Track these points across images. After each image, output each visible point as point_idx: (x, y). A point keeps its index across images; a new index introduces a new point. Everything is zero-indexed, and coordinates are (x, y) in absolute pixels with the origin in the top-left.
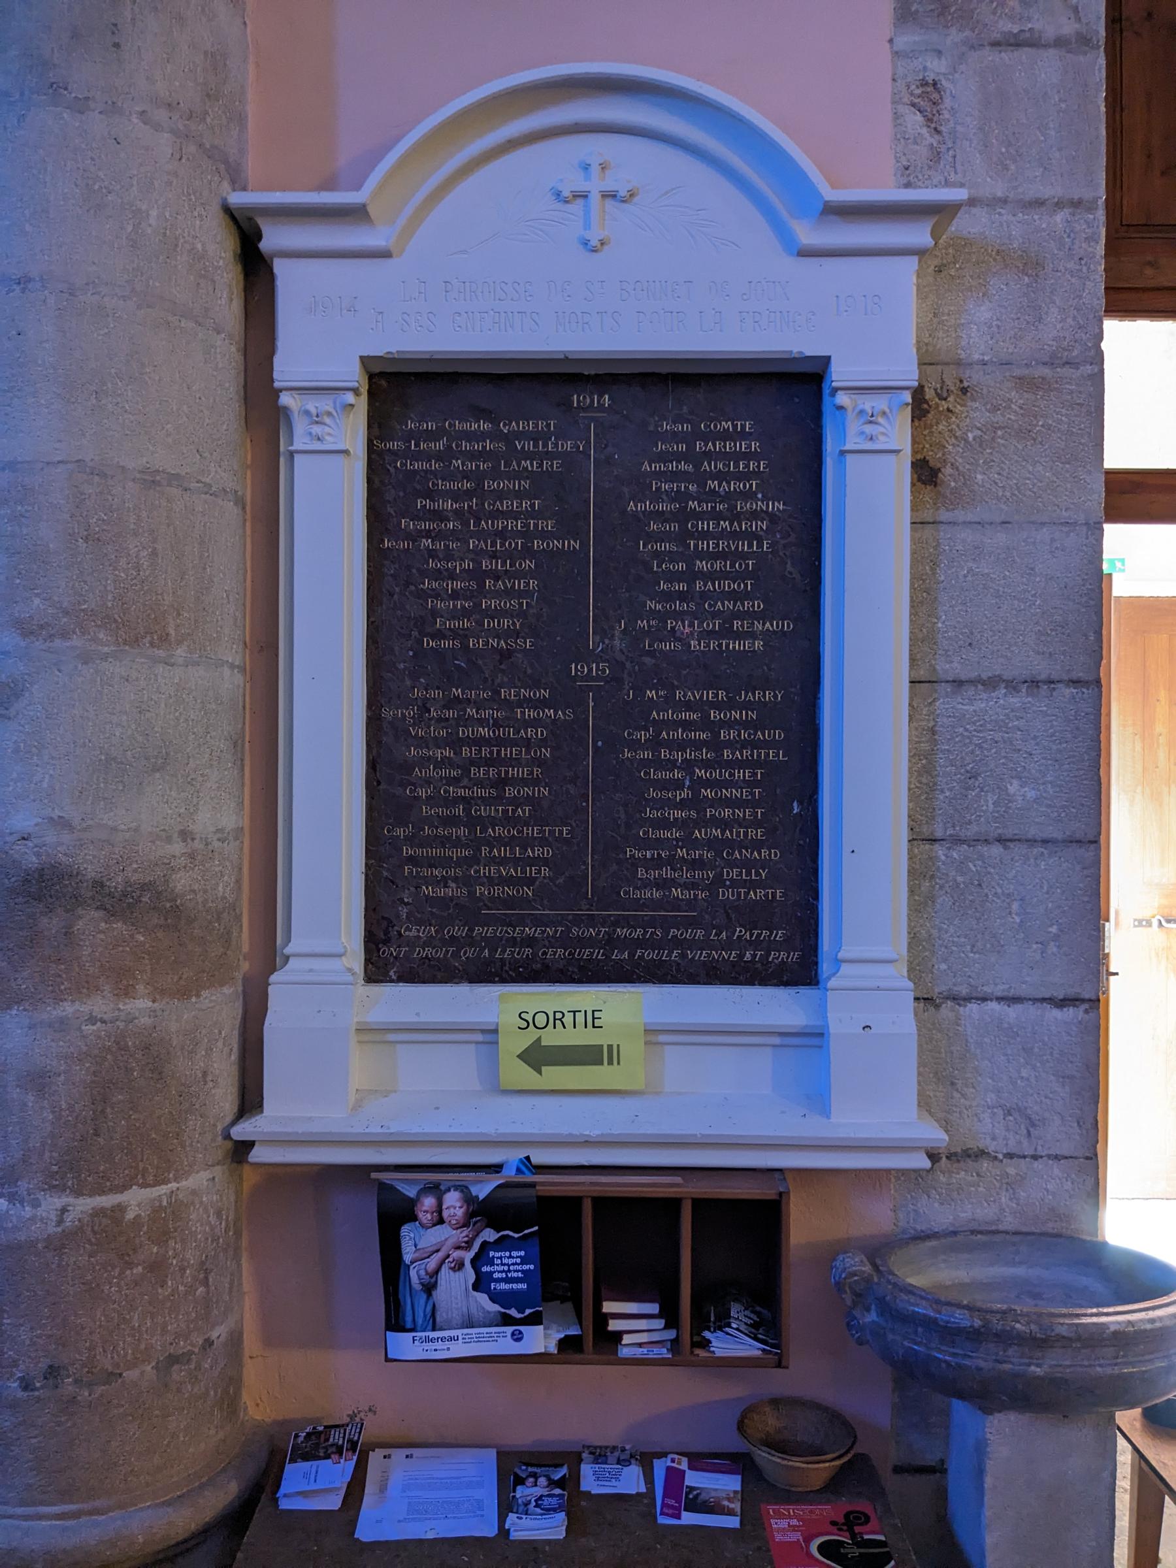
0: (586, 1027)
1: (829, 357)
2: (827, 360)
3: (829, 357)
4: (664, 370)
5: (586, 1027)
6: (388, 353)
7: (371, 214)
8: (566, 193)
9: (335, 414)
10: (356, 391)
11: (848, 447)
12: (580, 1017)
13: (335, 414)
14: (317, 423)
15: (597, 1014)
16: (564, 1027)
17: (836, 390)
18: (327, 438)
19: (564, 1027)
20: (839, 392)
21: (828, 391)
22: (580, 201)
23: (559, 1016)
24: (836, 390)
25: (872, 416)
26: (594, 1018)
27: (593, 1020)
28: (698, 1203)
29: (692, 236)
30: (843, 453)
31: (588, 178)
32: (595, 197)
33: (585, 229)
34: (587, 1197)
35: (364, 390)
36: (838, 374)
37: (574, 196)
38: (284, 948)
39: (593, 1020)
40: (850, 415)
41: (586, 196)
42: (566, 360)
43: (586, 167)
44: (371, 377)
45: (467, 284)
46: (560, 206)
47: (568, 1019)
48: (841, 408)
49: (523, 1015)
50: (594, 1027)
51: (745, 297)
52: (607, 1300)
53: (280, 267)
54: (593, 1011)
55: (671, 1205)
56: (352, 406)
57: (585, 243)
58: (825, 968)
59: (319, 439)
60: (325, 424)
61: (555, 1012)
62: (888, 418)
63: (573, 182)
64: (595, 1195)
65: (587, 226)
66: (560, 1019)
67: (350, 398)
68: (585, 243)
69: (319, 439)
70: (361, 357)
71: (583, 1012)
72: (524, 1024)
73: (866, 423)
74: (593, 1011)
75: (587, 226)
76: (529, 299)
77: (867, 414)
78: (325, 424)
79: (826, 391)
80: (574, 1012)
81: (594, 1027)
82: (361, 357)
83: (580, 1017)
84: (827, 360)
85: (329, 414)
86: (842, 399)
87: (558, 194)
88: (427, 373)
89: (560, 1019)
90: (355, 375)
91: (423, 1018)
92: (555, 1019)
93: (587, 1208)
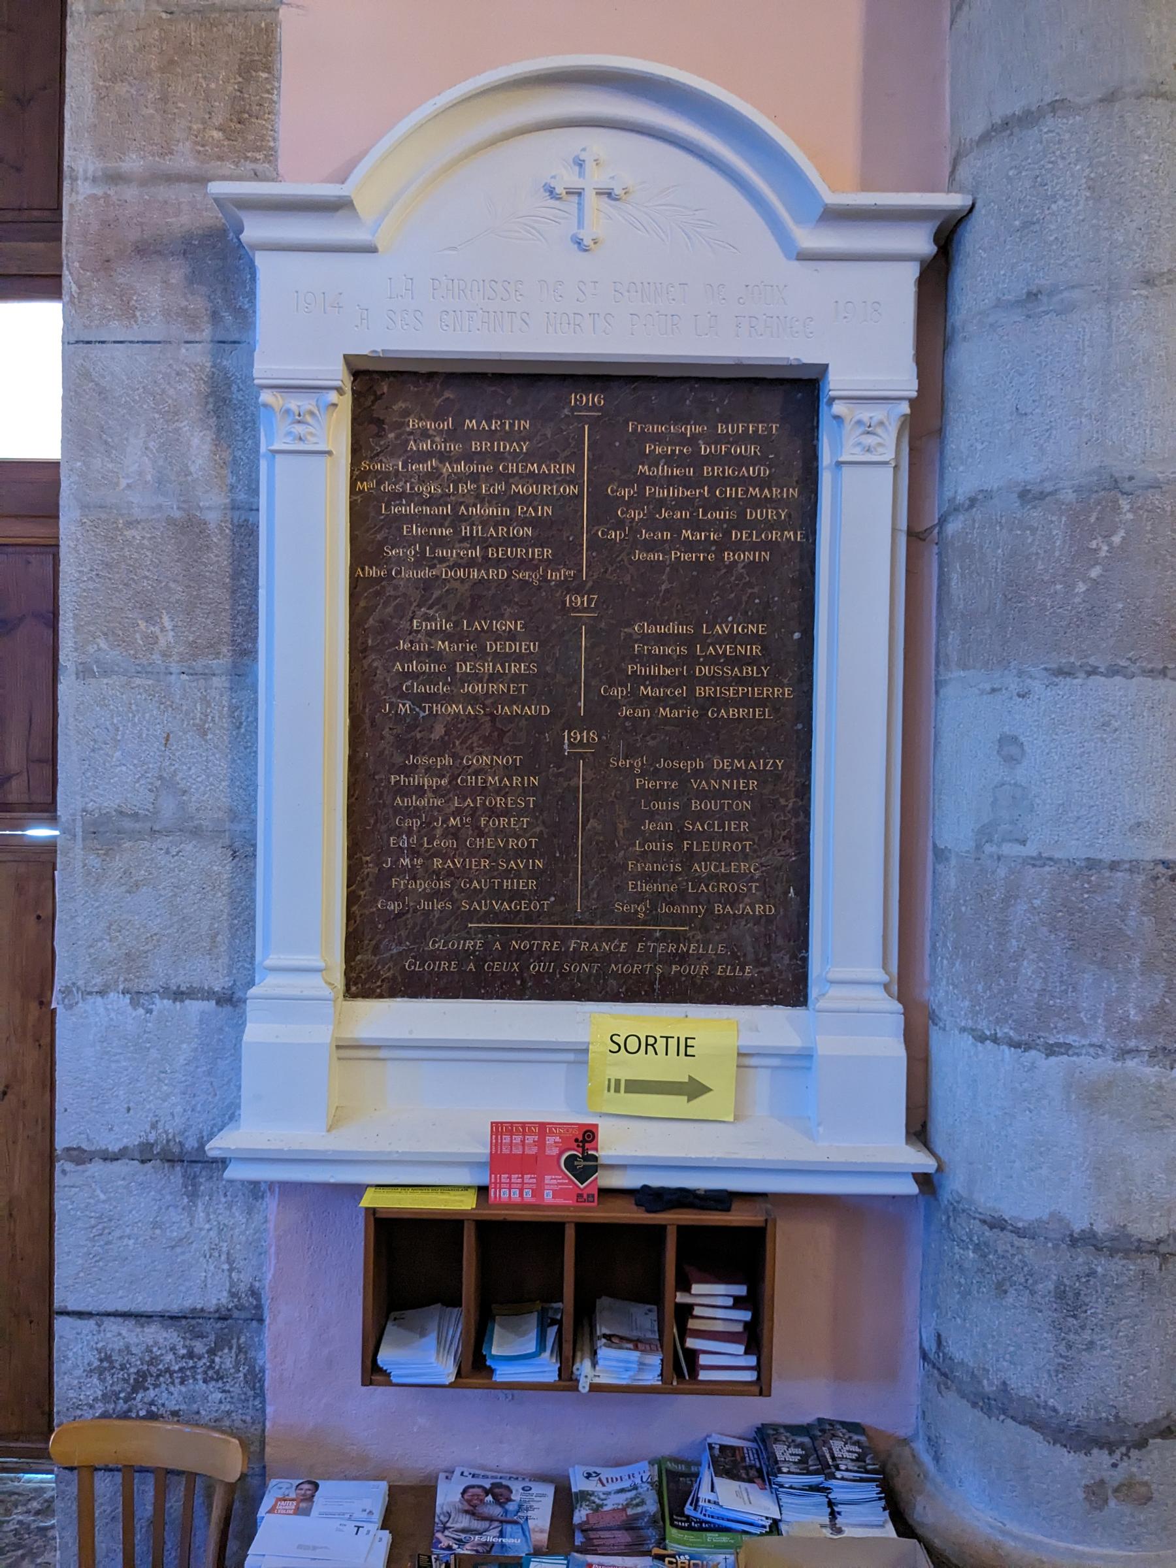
0: (678, 1055)
1: (827, 366)
2: (824, 368)
3: (827, 366)
4: (489, 370)
5: (678, 1055)
6: (374, 351)
7: (357, 207)
8: (560, 190)
9: (317, 412)
10: (339, 390)
11: (845, 458)
12: (673, 1043)
13: (317, 412)
14: (299, 422)
15: (690, 1042)
16: (656, 1054)
17: (833, 399)
18: (309, 437)
19: (656, 1054)
20: (837, 401)
21: (825, 400)
22: (575, 198)
23: (651, 1041)
24: (833, 399)
25: (870, 426)
26: (686, 1046)
27: (685, 1048)
28: (684, 1232)
29: (689, 238)
30: (839, 464)
31: (581, 174)
32: (590, 197)
33: (579, 228)
34: (569, 1222)
35: (348, 389)
36: (835, 383)
37: (567, 193)
38: (264, 960)
39: (685, 1048)
40: (848, 426)
41: (579, 194)
42: (739, 366)
43: (580, 163)
44: (356, 374)
45: (456, 281)
46: (553, 203)
47: (661, 1043)
48: (838, 418)
49: (614, 1038)
50: (686, 1055)
51: (741, 301)
52: (690, 1337)
53: (262, 260)
54: (686, 1039)
55: (554, 1230)
56: (335, 405)
57: (579, 242)
58: (813, 992)
59: (300, 439)
60: (308, 424)
61: (647, 1037)
62: (318, 420)
63: (568, 178)
64: (479, 1218)
65: (580, 224)
66: (652, 1045)
67: (333, 397)
68: (579, 242)
69: (300, 439)
70: (345, 356)
71: (676, 1039)
72: (616, 1048)
73: (294, 423)
74: (686, 1039)
75: (580, 224)
76: (519, 298)
77: (294, 413)
78: (308, 424)
79: (824, 401)
80: (667, 1038)
81: (686, 1055)
82: (345, 356)
83: (673, 1043)
84: (824, 368)
85: (312, 413)
86: (838, 408)
87: (551, 192)
88: (653, 377)
89: (652, 1045)
90: (340, 375)
91: (416, 1035)
92: (647, 1045)
93: (570, 1234)
